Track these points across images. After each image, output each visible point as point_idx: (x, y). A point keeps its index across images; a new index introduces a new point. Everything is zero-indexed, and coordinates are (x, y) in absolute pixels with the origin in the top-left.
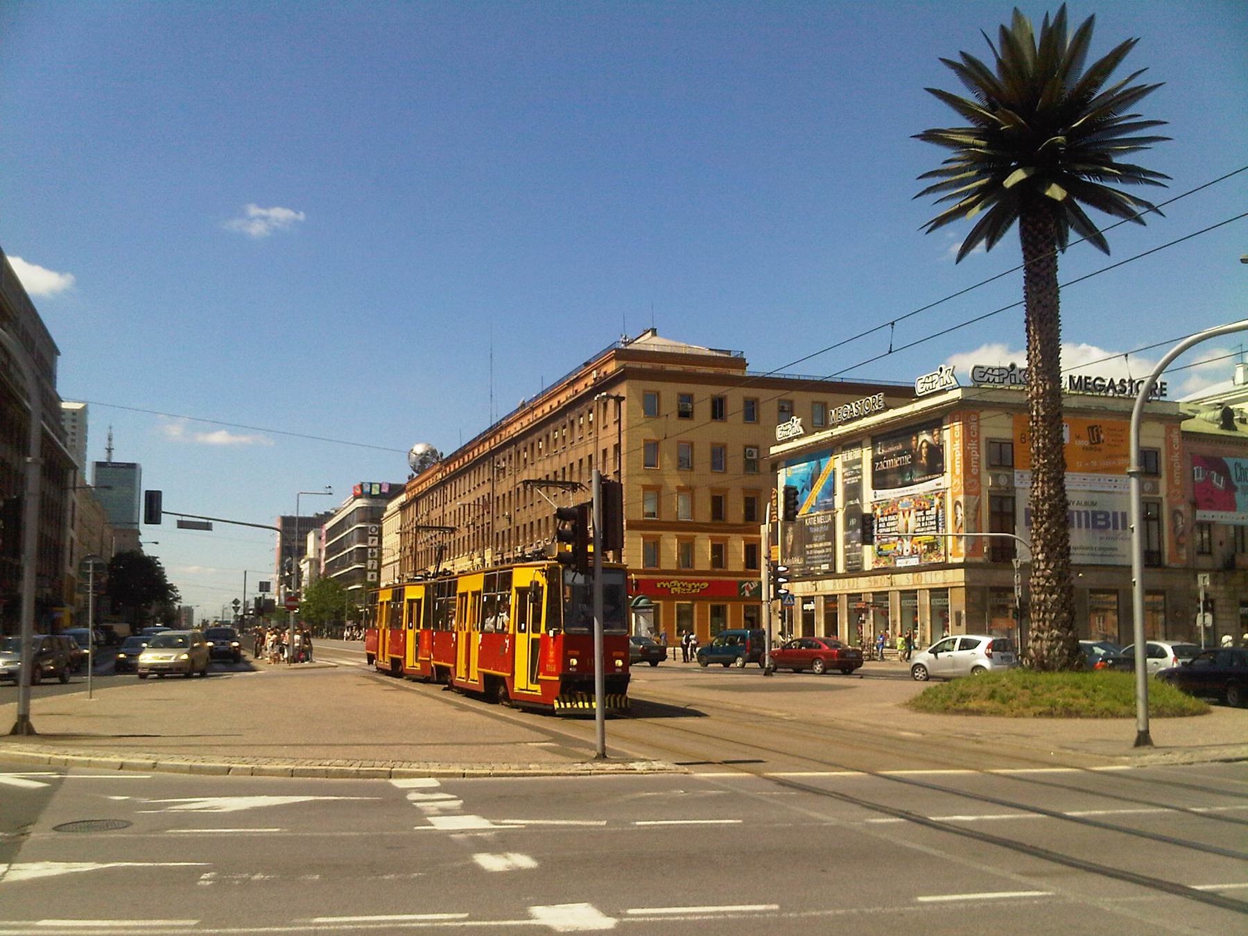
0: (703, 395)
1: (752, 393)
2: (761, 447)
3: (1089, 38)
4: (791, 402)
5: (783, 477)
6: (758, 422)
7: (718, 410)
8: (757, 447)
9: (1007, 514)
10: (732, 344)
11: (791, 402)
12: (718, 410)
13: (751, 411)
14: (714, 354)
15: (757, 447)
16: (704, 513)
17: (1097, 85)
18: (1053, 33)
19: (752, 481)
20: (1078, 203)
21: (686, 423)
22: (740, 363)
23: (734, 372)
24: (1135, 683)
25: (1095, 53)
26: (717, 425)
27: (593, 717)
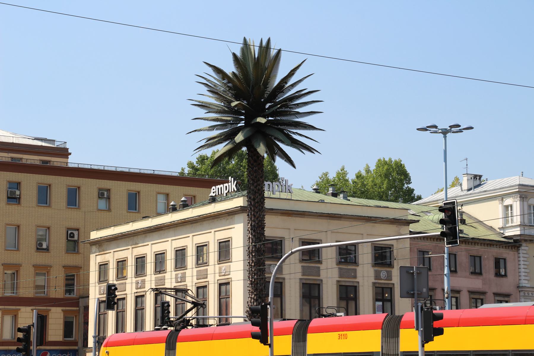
0: (30, 183)
1: (134, 186)
2: (82, 230)
3: (278, 63)
4: (108, 190)
5: (95, 260)
6: (79, 208)
7: (44, 195)
8: (78, 230)
9: (315, 298)
10: (59, 137)
11: (108, 190)
12: (44, 195)
13: (73, 198)
14: (39, 143)
15: (78, 230)
16: (58, 291)
17: (286, 83)
18: (265, 49)
19: (72, 260)
20: (282, 145)
21: (14, 208)
22: (64, 153)
23: (56, 161)
24: (145, 217)
25: (281, 73)
26: (44, 211)
27: (197, 315)
